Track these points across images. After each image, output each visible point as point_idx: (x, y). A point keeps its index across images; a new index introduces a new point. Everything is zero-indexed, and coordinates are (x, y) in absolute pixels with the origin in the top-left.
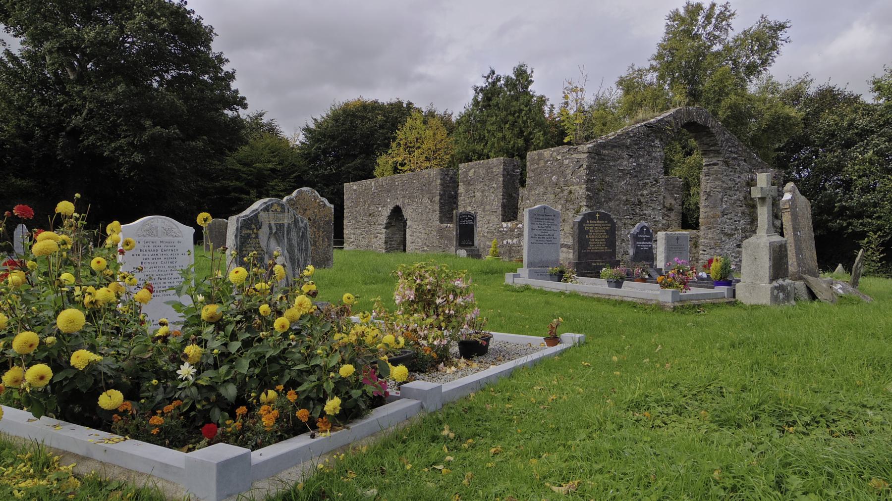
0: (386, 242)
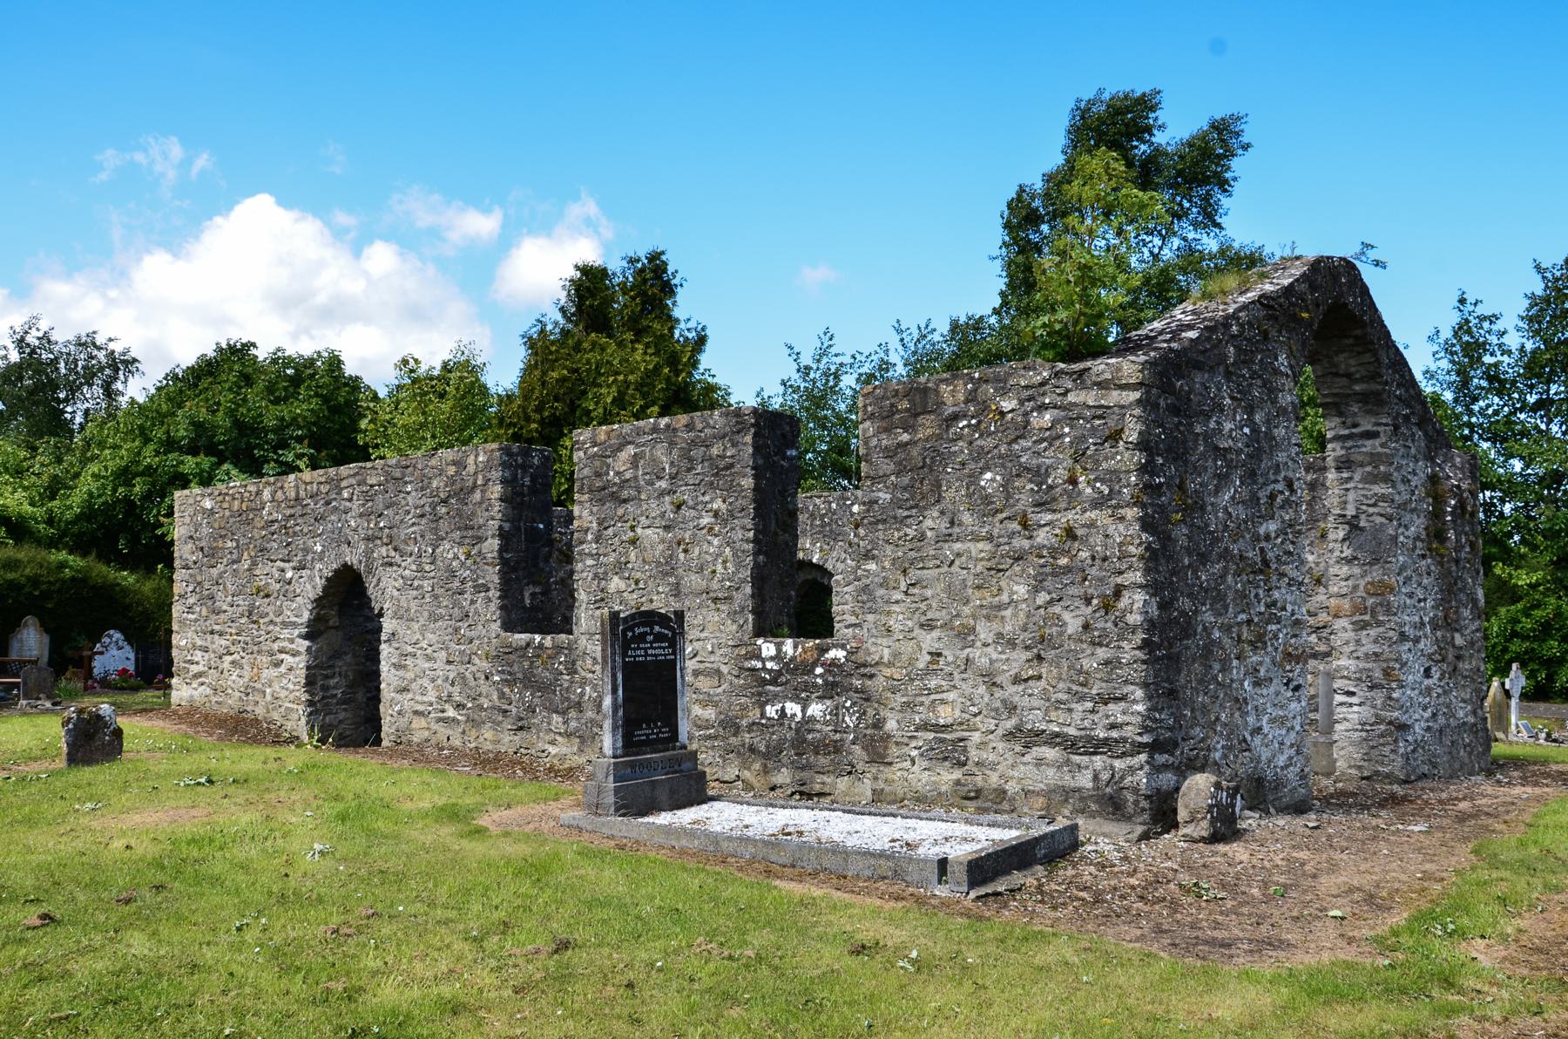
0: (310, 683)
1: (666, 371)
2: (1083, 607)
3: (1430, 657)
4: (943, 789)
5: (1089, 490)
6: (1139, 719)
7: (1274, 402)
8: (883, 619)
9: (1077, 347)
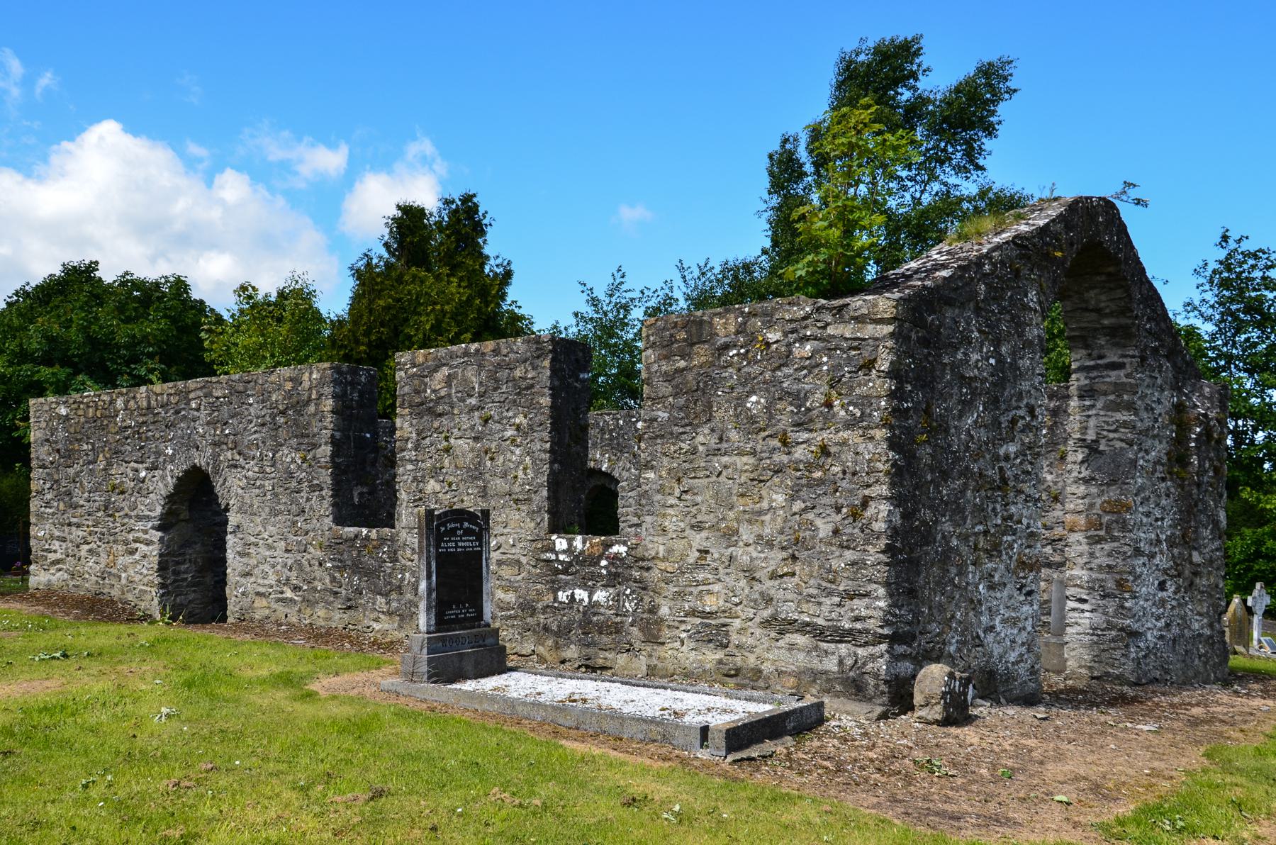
0: (162, 568)
1: (478, 302)
2: (834, 515)
3: (1165, 572)
4: (708, 666)
5: (843, 413)
6: (881, 613)
7: (1021, 335)
8: (660, 520)
9: (837, 284)
